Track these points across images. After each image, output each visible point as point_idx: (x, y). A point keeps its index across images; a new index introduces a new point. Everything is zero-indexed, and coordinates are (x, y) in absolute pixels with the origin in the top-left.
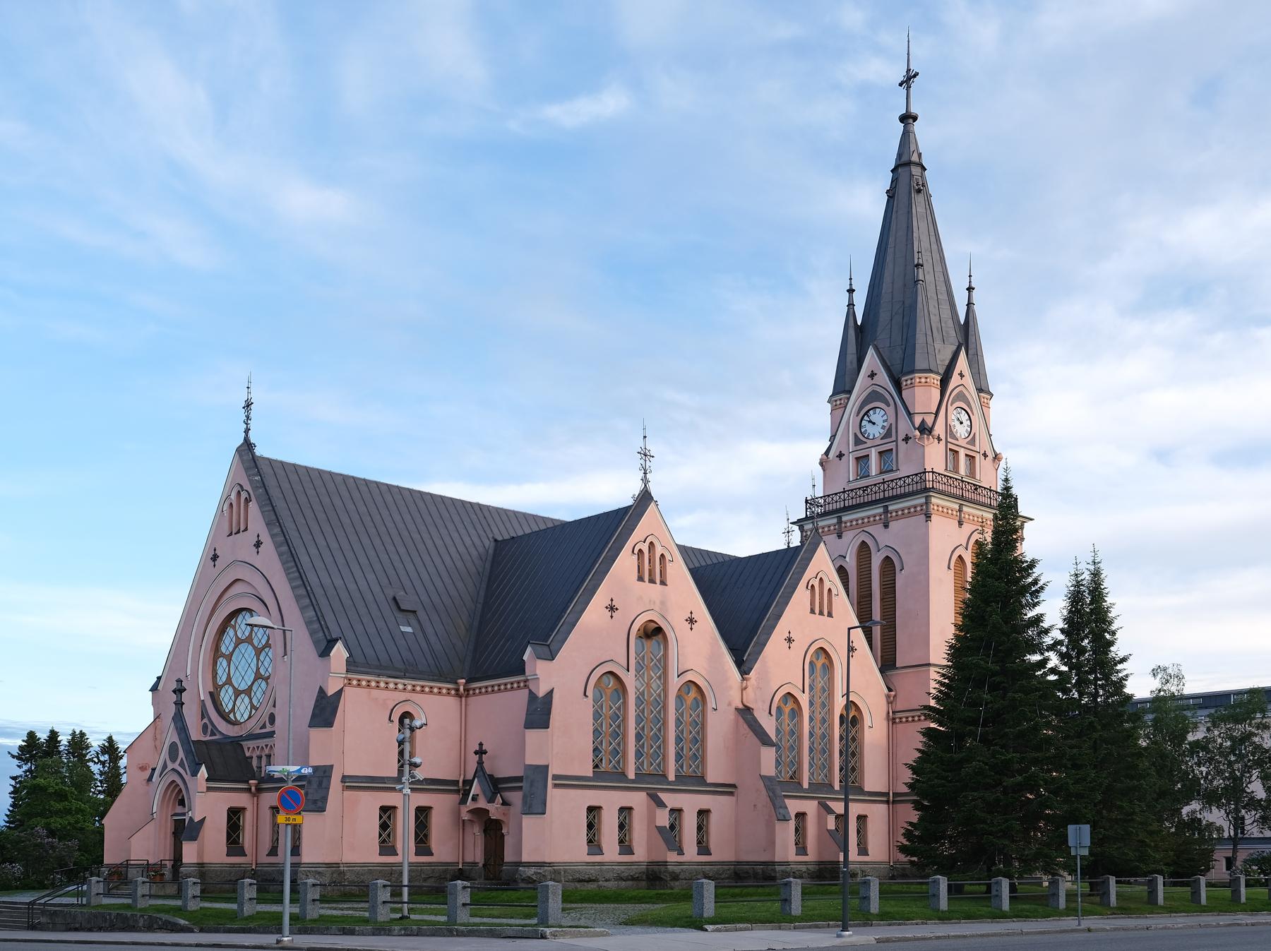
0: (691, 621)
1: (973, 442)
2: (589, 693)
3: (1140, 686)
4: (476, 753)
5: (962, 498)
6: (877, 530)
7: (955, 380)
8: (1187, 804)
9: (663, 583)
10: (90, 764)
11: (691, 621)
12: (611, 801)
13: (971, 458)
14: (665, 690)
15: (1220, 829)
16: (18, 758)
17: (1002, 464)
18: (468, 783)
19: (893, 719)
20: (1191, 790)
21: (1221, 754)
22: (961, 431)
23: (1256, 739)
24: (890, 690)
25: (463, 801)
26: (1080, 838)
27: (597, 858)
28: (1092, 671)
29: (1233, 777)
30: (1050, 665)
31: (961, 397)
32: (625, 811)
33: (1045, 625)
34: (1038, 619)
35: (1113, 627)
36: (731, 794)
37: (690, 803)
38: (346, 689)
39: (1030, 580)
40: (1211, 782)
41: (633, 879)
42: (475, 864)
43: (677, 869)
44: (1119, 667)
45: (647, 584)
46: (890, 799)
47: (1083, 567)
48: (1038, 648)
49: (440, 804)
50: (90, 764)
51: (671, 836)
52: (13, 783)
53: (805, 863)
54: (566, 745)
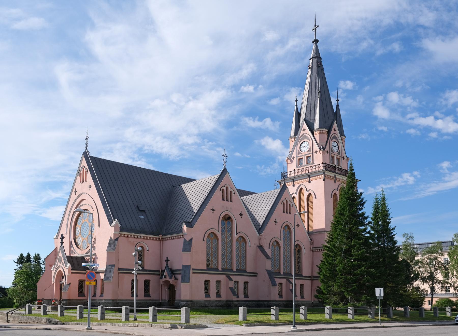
0: (241, 215)
1: (339, 153)
2: (205, 240)
3: (400, 240)
4: (166, 261)
5: (335, 173)
6: (307, 184)
7: (333, 132)
8: (415, 282)
9: (231, 201)
10: (41, 265)
11: (241, 215)
12: (213, 279)
13: (338, 159)
14: (232, 239)
15: (427, 291)
16: (17, 263)
17: (349, 162)
18: (163, 271)
19: (313, 250)
20: (417, 277)
21: (427, 264)
22: (335, 149)
23: (439, 259)
24: (311, 240)
25: (161, 278)
26: (379, 292)
27: (208, 299)
28: (382, 233)
29: (431, 273)
30: (367, 231)
31: (335, 137)
32: (218, 282)
33: (366, 216)
34: (363, 214)
35: (390, 217)
36: (256, 276)
37: (241, 279)
38: (120, 238)
39: (360, 200)
40: (424, 274)
41: (221, 306)
42: (165, 300)
43: (236, 303)
44: (392, 231)
45: (225, 202)
46: (312, 279)
47: (378, 196)
48: (363, 224)
49: (153, 279)
50: (41, 265)
51: (234, 291)
52: (15, 271)
53: (282, 301)
54: (198, 258)
